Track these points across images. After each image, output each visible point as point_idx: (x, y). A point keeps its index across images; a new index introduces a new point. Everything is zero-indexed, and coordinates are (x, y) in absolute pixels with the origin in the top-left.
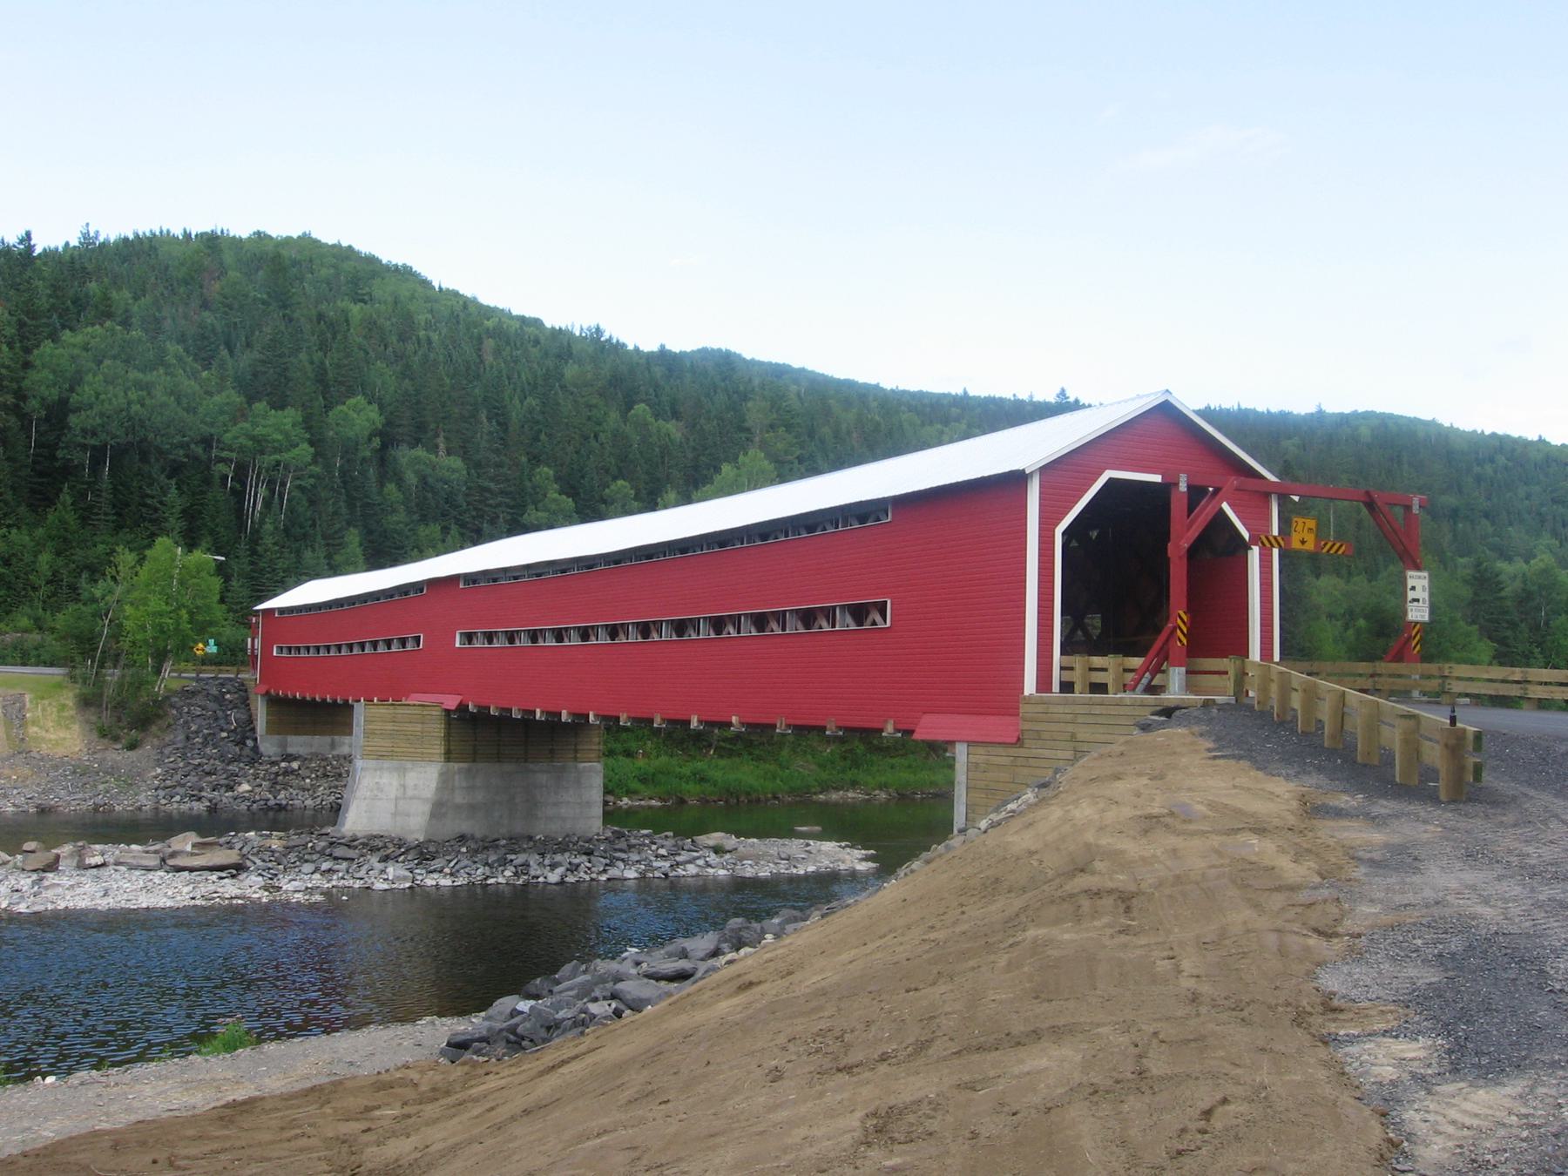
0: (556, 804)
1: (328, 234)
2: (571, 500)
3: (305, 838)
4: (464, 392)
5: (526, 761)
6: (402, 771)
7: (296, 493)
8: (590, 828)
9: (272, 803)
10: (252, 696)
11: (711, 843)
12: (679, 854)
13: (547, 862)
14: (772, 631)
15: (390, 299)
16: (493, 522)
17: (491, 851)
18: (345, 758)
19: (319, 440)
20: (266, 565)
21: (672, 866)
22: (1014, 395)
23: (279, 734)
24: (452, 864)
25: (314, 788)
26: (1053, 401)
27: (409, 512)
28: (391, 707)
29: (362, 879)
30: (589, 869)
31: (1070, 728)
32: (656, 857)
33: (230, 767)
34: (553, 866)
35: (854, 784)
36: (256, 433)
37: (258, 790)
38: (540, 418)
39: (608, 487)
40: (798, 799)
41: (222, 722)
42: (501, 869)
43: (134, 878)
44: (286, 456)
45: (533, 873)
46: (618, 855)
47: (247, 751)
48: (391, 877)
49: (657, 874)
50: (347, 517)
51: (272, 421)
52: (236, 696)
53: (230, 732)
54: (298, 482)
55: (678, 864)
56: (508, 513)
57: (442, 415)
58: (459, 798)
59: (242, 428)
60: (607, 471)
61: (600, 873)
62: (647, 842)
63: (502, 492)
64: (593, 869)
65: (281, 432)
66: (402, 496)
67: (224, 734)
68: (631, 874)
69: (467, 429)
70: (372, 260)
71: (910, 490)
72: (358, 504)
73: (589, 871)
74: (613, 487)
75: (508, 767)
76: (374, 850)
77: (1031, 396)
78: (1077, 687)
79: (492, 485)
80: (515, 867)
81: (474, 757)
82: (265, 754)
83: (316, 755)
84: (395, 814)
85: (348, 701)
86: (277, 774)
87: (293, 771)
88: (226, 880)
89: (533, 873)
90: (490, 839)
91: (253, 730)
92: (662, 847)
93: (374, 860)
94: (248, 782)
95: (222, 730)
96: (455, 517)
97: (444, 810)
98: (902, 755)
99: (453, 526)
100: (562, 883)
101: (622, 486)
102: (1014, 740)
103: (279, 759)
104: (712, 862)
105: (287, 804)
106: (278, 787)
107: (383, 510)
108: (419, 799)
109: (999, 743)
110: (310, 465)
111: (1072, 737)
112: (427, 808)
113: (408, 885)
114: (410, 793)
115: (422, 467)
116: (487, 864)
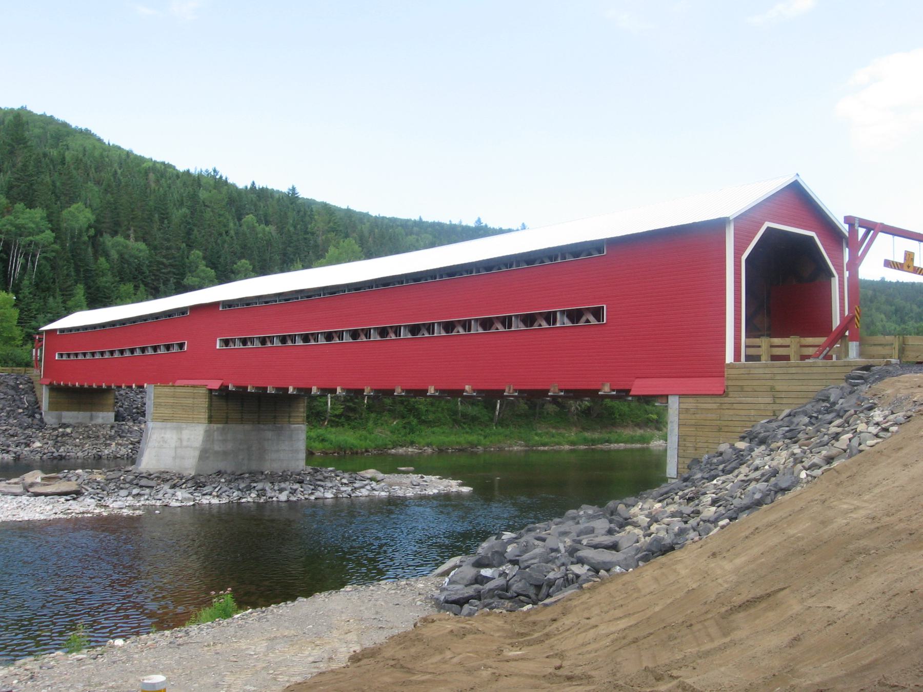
0: (278, 451)
1: (38, 108)
2: (213, 271)
3: (118, 474)
4: (144, 203)
5: (259, 423)
6: (179, 429)
7: (43, 262)
8: (298, 466)
9: (56, 454)
10: (37, 386)
11: (369, 476)
12: (355, 483)
13: (276, 488)
14: (497, 329)
15: (81, 149)
16: (166, 282)
17: (240, 481)
18: (100, 426)
19: (57, 229)
20: (24, 306)
21: (352, 490)
22: (450, 221)
23: (57, 410)
24: (217, 489)
25: (83, 445)
26: (474, 226)
27: (114, 276)
28: (172, 388)
29: (160, 500)
30: (302, 492)
31: (770, 383)
32: (342, 484)
33: (26, 432)
34: (281, 490)
35: (412, 443)
36: (17, 222)
37: (46, 446)
38: (190, 221)
39: (236, 264)
40: (380, 452)
41: (18, 403)
42: (249, 492)
43: (9, 501)
44: (38, 238)
45: (269, 495)
46: (319, 483)
47: (36, 422)
48: (180, 498)
49: (345, 495)
50: (75, 277)
51: (27, 216)
52: (26, 386)
53: (24, 409)
54: (44, 255)
55: (356, 489)
56: (175, 278)
57: (131, 216)
58: (217, 447)
59: (8, 220)
60: (235, 254)
61: (310, 494)
62: (333, 475)
63: (172, 266)
64: (305, 492)
65: (34, 222)
66: (109, 266)
67: (21, 411)
68: (329, 495)
69: (147, 226)
70: (65, 125)
71: (416, 271)
72: (82, 270)
73: (304, 494)
74: (239, 264)
75: (247, 427)
76: (165, 481)
77: (461, 222)
78: (763, 358)
79: (165, 261)
80: (257, 491)
81: (226, 421)
82: (48, 423)
83: (81, 424)
84: (175, 458)
85: (111, 386)
86: (57, 436)
87: (68, 434)
88: (71, 502)
89: (269, 495)
90: (239, 473)
91: (39, 408)
92: (344, 478)
93: (166, 487)
94: (39, 441)
95: (19, 408)
96: (141, 279)
97: (207, 455)
98: (438, 426)
99: (141, 285)
100: (288, 501)
101: (245, 263)
102: (721, 392)
103: (57, 426)
104: (375, 487)
105: (65, 456)
106: (59, 444)
107: (97, 274)
108: (191, 447)
109: (713, 395)
110: (52, 244)
111: (771, 389)
112: (197, 453)
113: (192, 503)
114: (185, 443)
115: (121, 248)
116: (239, 490)
